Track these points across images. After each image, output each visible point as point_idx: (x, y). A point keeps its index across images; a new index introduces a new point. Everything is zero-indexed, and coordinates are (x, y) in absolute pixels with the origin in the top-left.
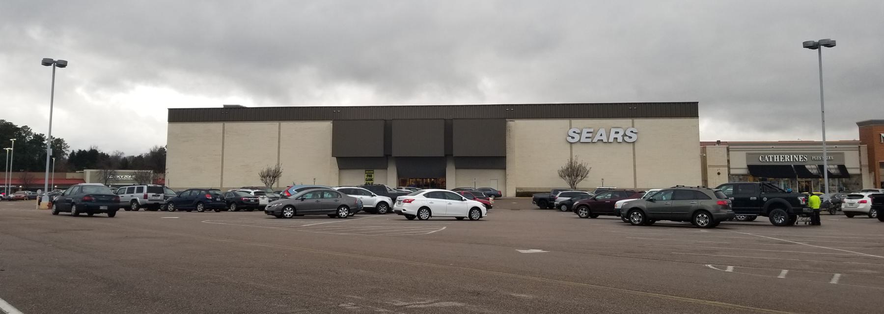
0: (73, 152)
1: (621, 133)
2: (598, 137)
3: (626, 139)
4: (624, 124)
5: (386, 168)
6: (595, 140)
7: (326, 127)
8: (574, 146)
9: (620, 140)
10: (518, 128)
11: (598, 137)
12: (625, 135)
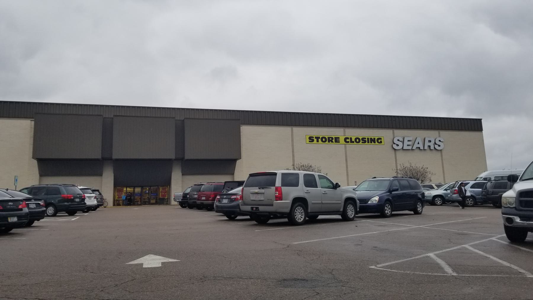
0: (142, 264)
1: (433, 142)
2: (416, 145)
3: (436, 147)
4: (431, 135)
5: (101, 175)
6: (414, 148)
7: (24, 127)
8: (397, 153)
9: (432, 148)
10: (248, 133)
11: (416, 145)
12: (435, 143)
